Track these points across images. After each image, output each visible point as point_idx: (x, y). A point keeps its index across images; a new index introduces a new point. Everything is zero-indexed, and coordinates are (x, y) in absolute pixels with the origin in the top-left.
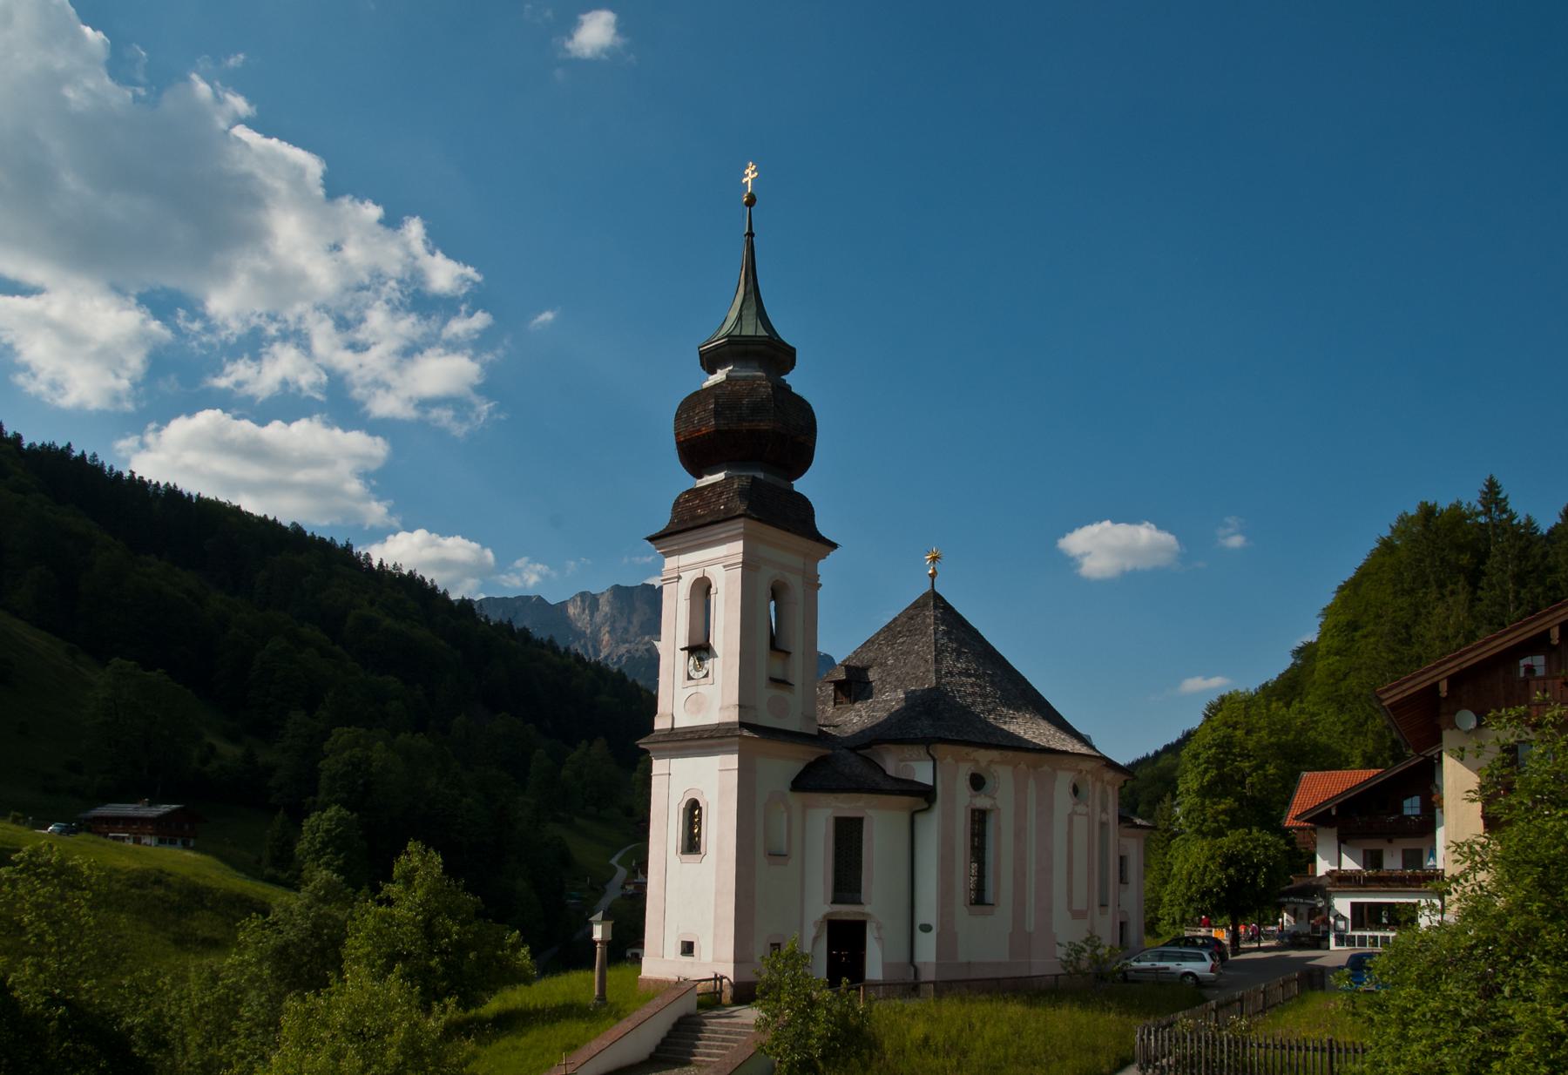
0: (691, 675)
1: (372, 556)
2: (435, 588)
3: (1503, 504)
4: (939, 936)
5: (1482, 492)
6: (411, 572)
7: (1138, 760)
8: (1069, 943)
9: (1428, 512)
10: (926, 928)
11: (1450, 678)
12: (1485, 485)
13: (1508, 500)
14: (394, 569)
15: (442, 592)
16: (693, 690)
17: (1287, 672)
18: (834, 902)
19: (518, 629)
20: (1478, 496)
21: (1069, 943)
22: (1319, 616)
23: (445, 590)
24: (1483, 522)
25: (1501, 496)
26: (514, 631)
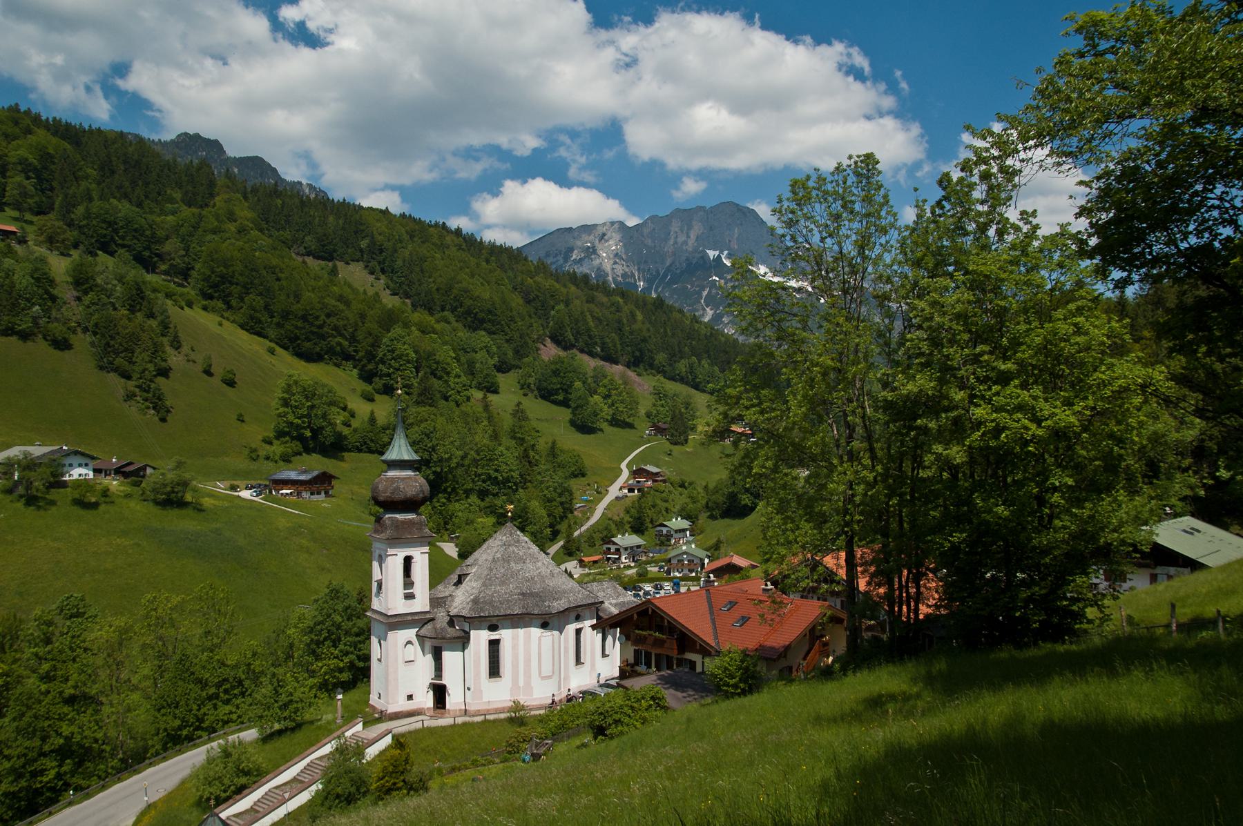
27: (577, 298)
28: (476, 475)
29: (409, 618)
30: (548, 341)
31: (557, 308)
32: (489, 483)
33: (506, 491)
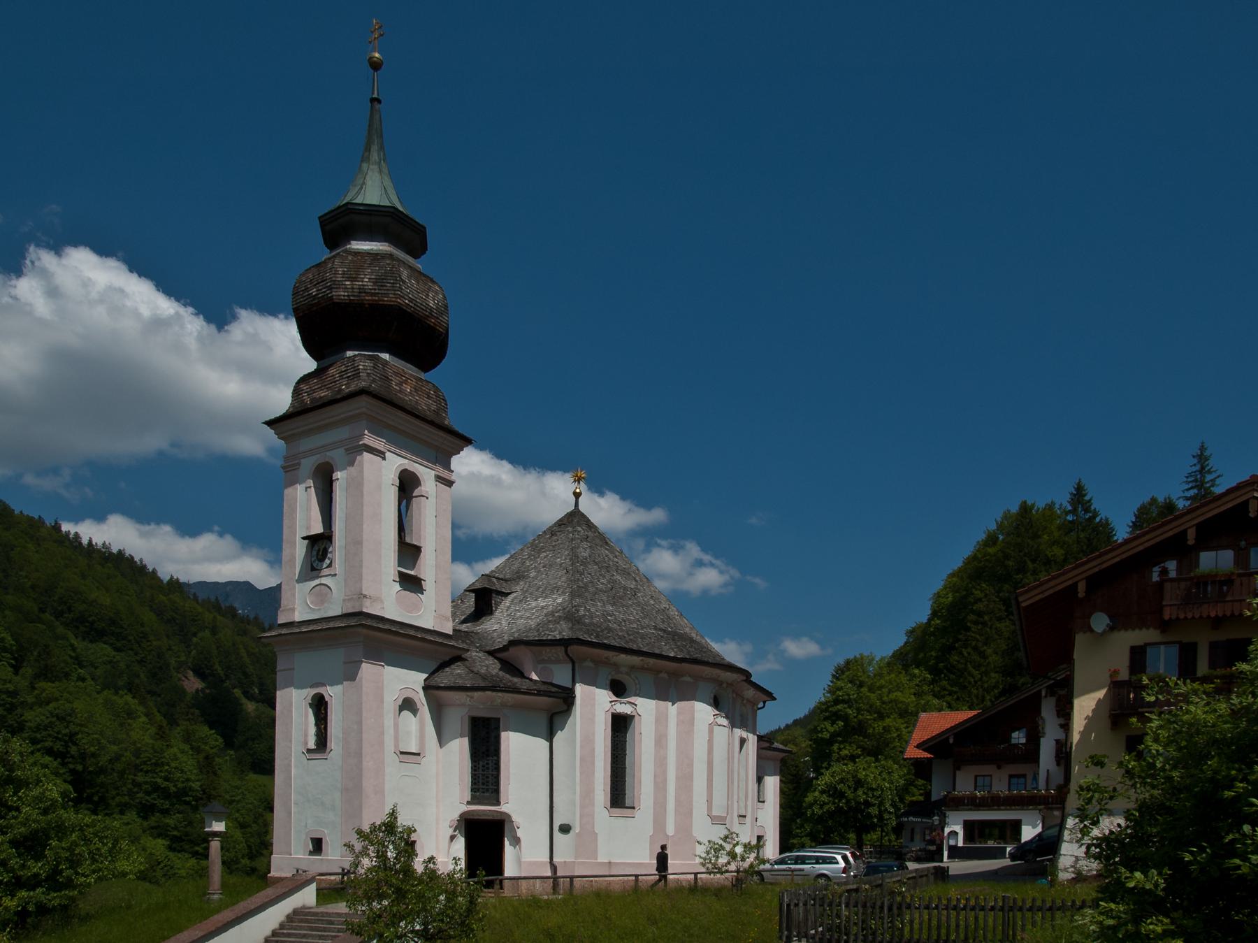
0: (315, 565)
1: (81, 535)
2: (144, 567)
3: (1088, 504)
5: (1071, 494)
7: (772, 731)
8: (709, 842)
9: (1025, 509)
11: (1089, 579)
12: (1074, 488)
13: (1092, 501)
14: (103, 547)
15: (151, 570)
17: (901, 648)
18: (468, 803)
20: (1068, 497)
21: (709, 842)
22: (930, 600)
23: (154, 569)
24: (1071, 519)
25: (1087, 498)
27: (23, 866)
28: (135, 784)
29: (412, 632)
30: (191, 673)
31: (200, 635)
32: (154, 795)
33: (181, 808)
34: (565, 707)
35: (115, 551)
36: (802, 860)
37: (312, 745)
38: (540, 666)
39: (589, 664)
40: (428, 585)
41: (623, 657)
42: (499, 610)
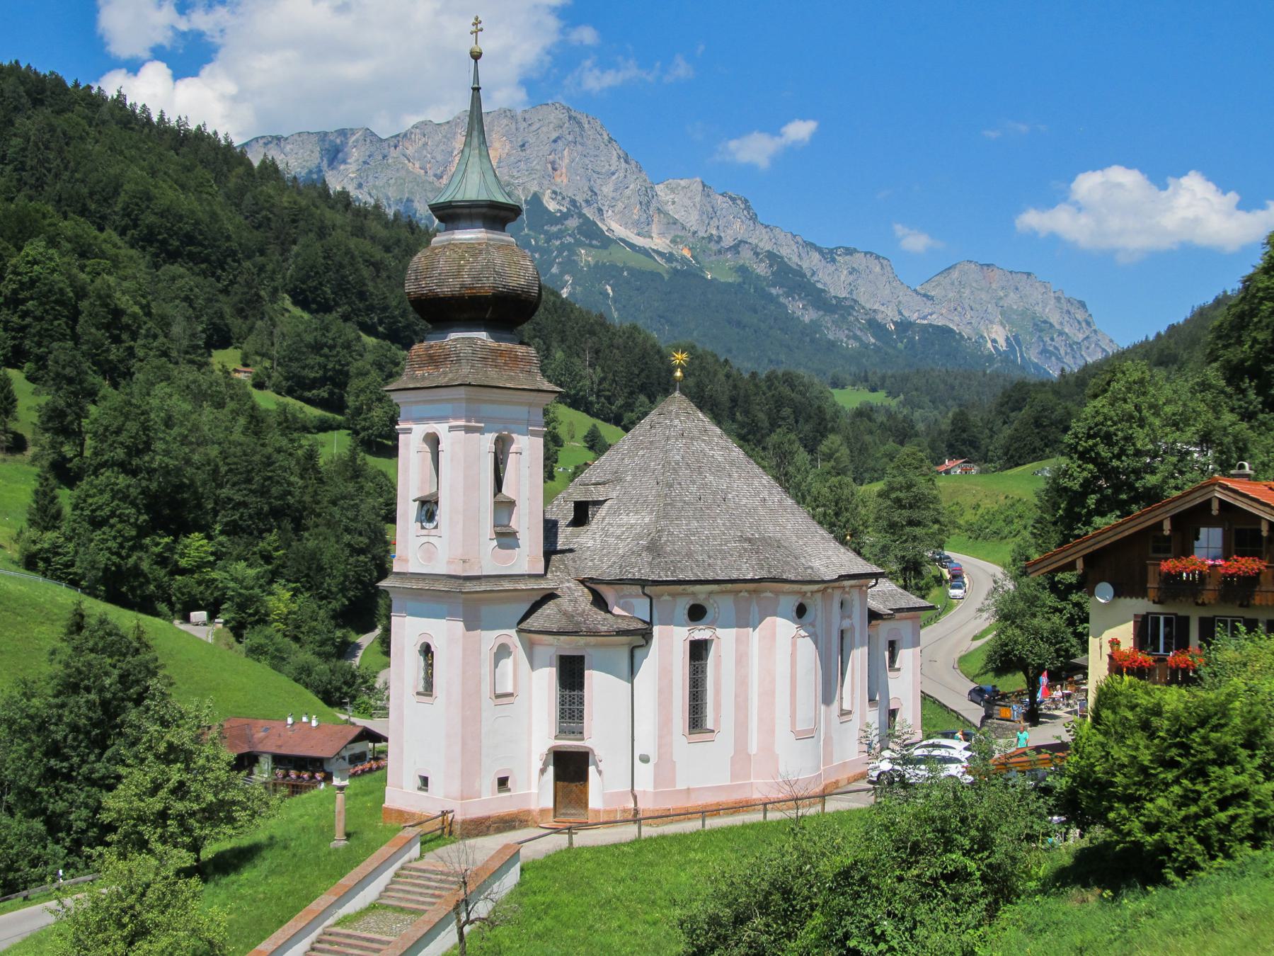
2: (229, 145)
4: (656, 765)
6: (199, 128)
10: (645, 759)
11: (1174, 519)
16: (425, 539)
18: (556, 737)
19: (334, 192)
26: (329, 193)
34: (643, 642)
35: (192, 127)
36: (934, 746)
37: (421, 689)
38: (622, 601)
39: (666, 598)
40: (523, 537)
41: (698, 588)
42: (595, 521)
